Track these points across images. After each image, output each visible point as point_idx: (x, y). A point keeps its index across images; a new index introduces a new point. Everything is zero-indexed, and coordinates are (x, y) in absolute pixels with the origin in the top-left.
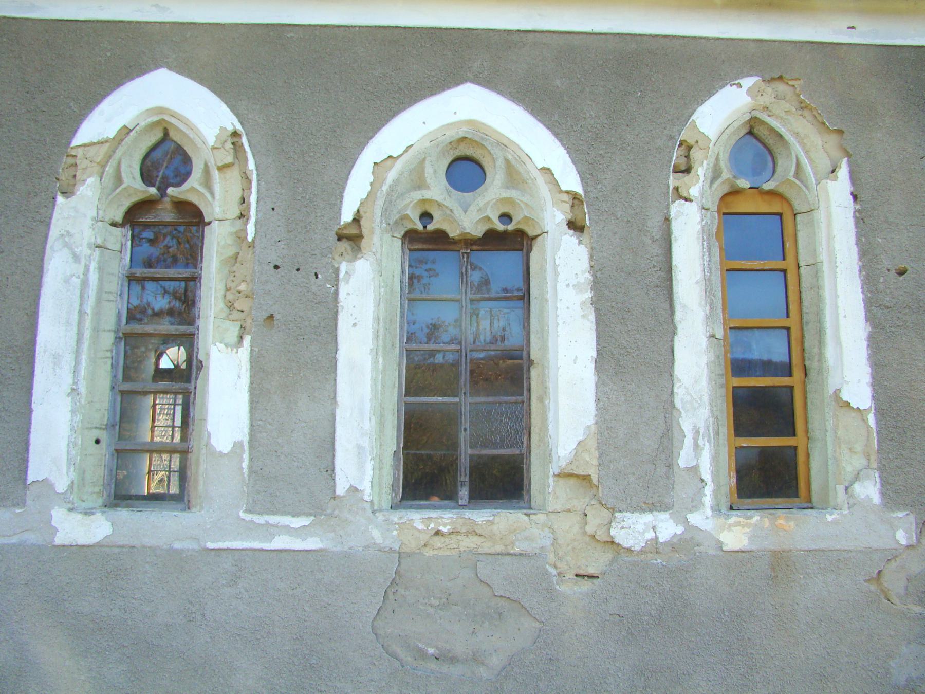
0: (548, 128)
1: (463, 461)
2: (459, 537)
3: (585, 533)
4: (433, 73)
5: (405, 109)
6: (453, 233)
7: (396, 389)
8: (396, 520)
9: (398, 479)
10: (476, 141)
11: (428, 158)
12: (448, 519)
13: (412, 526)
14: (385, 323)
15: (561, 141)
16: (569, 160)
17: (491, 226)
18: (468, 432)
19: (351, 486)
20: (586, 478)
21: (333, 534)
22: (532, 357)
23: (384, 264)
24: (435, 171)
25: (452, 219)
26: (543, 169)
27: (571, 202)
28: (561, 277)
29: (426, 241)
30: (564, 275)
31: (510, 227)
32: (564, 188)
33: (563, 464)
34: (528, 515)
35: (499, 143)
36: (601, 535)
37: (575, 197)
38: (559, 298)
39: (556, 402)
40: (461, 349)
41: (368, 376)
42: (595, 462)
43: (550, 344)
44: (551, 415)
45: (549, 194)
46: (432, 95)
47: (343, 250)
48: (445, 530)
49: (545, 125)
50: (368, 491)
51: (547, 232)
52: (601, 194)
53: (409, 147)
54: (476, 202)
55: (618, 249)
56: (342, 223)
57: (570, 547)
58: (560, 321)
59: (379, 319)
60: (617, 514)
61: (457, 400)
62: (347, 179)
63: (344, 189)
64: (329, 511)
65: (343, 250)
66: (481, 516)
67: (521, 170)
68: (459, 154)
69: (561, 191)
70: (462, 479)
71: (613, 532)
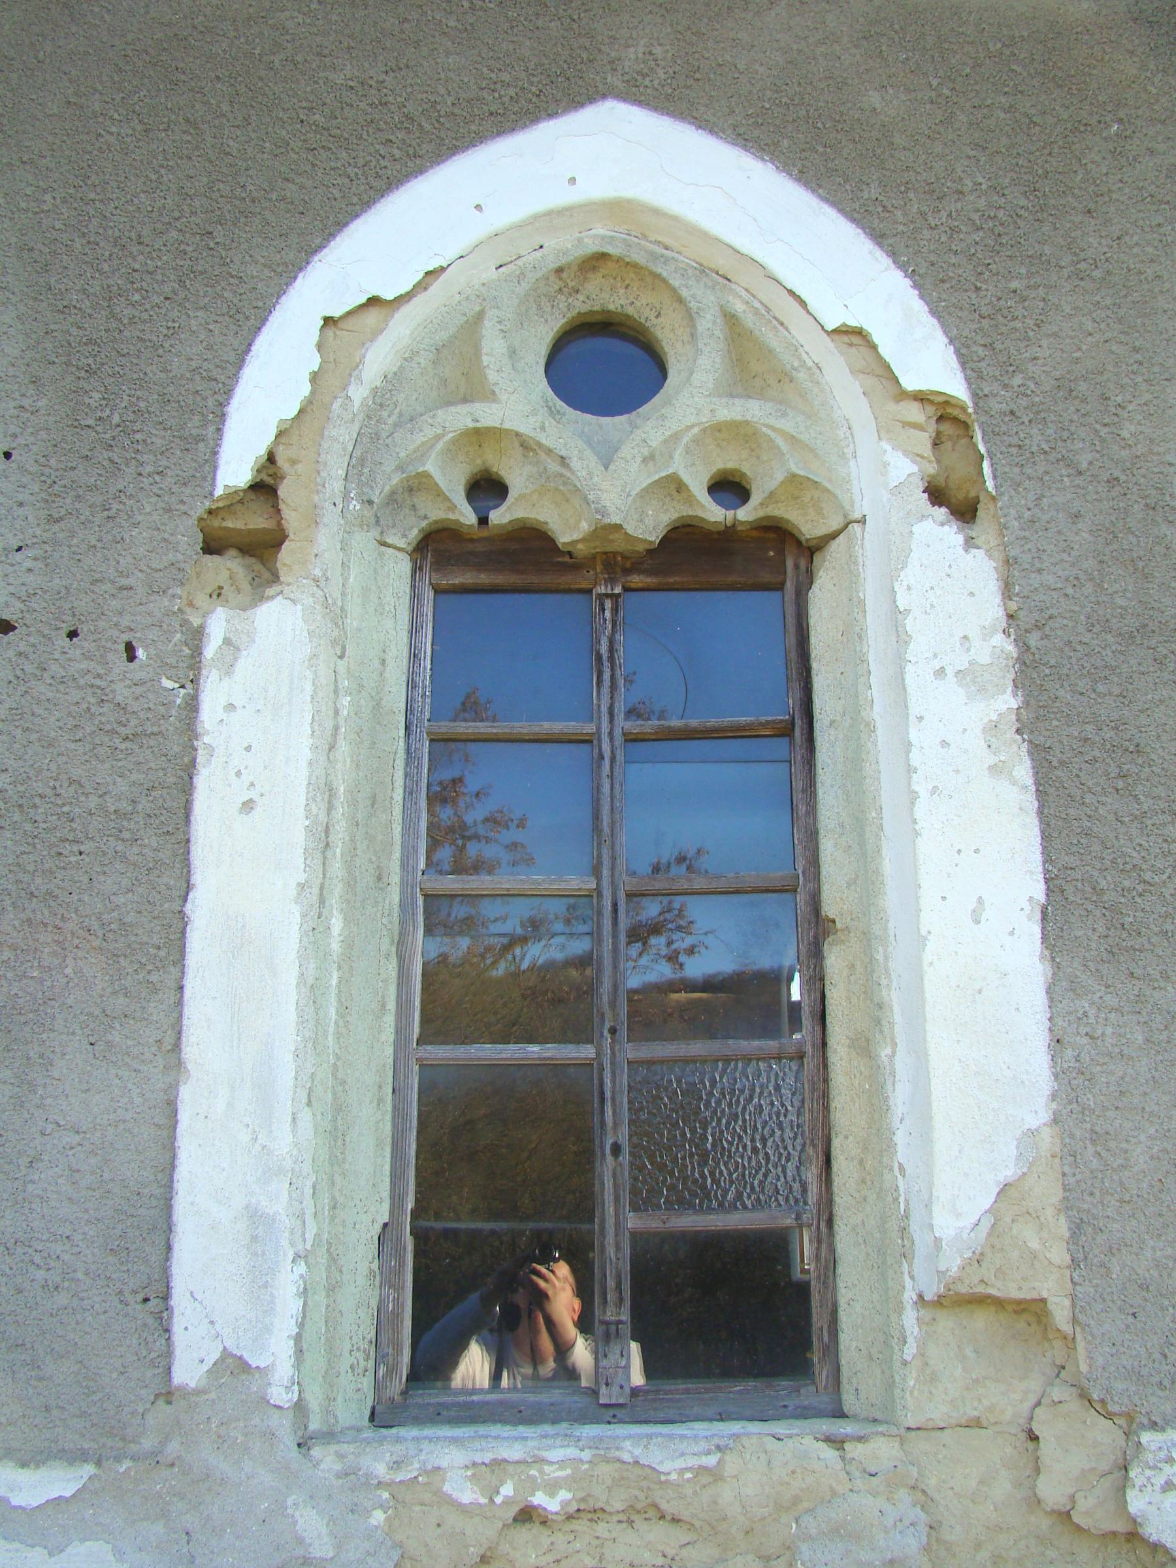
0: (853, 220)
1: (611, 1251)
2: (601, 1529)
3: (1035, 1501)
4: (506, 77)
5: (421, 171)
6: (569, 530)
7: (390, 1020)
8: (381, 1470)
9: (397, 1315)
10: (634, 266)
11: (491, 313)
12: (562, 1464)
13: (439, 1492)
14: (353, 803)
15: (893, 254)
16: (919, 307)
17: (687, 511)
18: (625, 1157)
19: (226, 1354)
20: (1033, 1311)
21: (159, 1528)
22: (829, 909)
23: (352, 623)
24: (512, 353)
27: (932, 427)
28: (918, 649)
29: (485, 562)
30: (926, 640)
31: (745, 514)
32: (910, 383)
33: (952, 1263)
34: (836, 1442)
35: (703, 270)
36: (1092, 1510)
37: (946, 416)
38: (914, 710)
39: (920, 1055)
40: (599, 890)
41: (289, 975)
42: (1059, 1254)
43: (888, 867)
44: (900, 1097)
45: (864, 403)
46: (500, 133)
47: (223, 578)
48: (550, 1503)
49: (841, 211)
50: (284, 1369)
51: (862, 521)
52: (1024, 402)
53: (432, 275)
54: (638, 435)
55: (1090, 564)
56: (219, 492)
57: (984, 1555)
58: (921, 786)
59: (331, 791)
60: (1146, 1437)
61: (587, 1052)
62: (240, 364)
63: (229, 393)
64: (148, 1443)
65: (223, 578)
66: (674, 1452)
67: (774, 343)
68: (585, 308)
69: (903, 395)
70: (610, 1315)
71: (1136, 1503)
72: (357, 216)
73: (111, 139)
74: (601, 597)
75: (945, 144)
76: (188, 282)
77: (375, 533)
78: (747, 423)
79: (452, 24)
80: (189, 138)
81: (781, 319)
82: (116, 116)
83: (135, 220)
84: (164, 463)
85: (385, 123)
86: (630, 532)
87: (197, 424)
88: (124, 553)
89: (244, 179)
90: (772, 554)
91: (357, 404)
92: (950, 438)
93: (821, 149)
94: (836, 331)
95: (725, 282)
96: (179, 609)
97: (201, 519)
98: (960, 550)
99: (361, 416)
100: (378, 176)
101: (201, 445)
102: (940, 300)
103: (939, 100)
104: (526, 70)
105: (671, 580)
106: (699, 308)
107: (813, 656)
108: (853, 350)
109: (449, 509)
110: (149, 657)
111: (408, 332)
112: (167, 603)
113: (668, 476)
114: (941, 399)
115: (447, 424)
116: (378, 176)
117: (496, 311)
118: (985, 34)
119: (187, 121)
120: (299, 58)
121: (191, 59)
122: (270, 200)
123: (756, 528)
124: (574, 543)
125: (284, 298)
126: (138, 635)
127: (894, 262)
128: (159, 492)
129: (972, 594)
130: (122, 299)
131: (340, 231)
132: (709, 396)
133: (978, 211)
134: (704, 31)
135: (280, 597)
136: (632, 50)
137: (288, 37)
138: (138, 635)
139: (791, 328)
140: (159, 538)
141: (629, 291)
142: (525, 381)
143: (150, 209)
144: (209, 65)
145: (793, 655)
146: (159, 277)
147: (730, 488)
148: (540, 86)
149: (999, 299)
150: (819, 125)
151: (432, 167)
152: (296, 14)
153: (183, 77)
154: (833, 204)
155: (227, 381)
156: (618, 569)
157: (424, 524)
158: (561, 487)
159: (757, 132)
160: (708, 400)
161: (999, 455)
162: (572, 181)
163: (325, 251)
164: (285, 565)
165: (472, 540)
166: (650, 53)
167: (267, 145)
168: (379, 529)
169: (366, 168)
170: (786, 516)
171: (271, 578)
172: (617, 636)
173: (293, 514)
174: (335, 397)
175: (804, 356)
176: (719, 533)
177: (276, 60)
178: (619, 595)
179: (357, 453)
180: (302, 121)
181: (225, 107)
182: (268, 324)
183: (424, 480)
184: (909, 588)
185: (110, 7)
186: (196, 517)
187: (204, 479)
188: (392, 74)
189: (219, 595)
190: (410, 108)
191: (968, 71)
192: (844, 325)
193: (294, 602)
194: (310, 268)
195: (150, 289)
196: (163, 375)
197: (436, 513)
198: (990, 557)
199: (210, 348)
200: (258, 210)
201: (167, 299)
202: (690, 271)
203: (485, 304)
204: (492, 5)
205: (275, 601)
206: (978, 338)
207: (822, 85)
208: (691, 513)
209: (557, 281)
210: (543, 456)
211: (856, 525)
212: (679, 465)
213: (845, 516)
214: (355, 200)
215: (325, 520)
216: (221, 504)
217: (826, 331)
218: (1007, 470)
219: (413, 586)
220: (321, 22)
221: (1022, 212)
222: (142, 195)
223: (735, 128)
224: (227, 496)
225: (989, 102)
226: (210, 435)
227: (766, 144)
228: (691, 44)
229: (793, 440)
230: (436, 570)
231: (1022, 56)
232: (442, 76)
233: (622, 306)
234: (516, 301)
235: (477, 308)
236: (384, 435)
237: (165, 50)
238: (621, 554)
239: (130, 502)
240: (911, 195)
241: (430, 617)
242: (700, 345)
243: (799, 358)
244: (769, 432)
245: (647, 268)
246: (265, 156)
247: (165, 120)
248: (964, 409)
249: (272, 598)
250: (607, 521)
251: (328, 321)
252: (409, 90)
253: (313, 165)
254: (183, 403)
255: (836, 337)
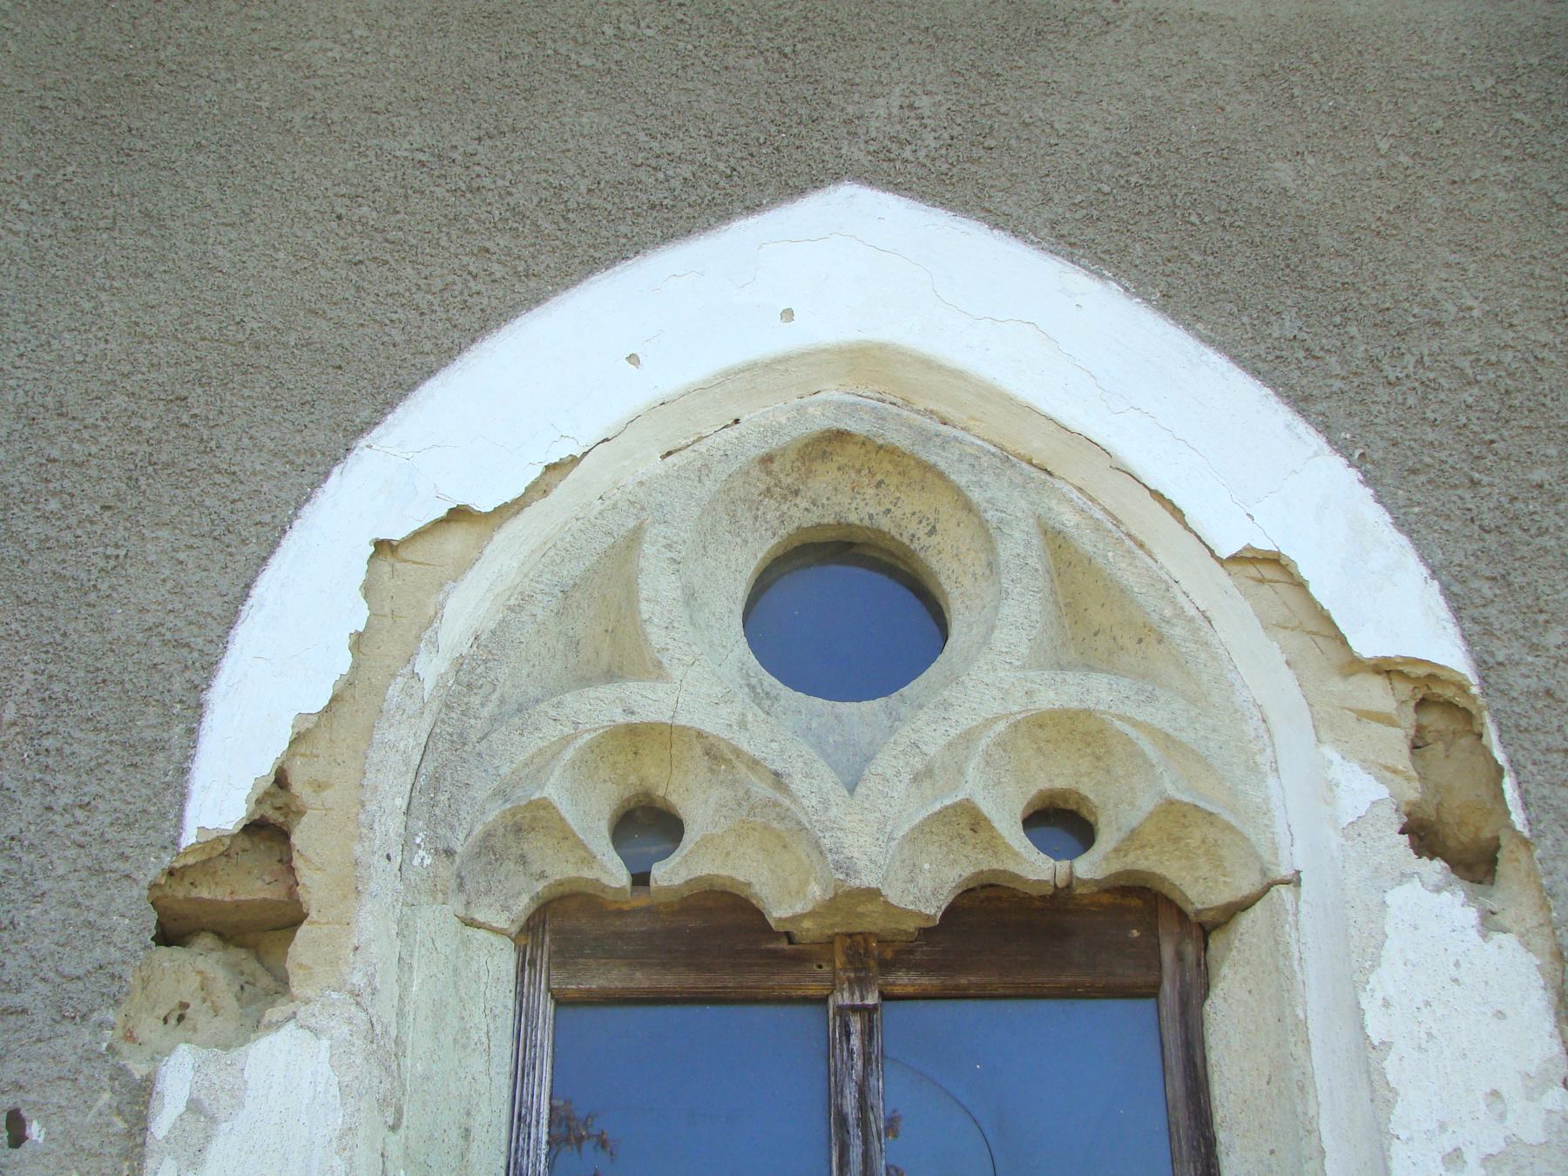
0: (1256, 373)
4: (675, 146)
5: (538, 299)
6: (789, 897)
10: (891, 452)
11: (654, 532)
15: (1325, 428)
16: (1376, 517)
17: (988, 863)
23: (414, 1065)
24: (690, 597)
25: (781, 826)
26: (1247, 559)
27: (1409, 718)
31: (1089, 867)
32: (1367, 645)
35: (1006, 458)
37: (1430, 698)
45: (1287, 677)
46: (668, 237)
49: (1235, 359)
51: (1295, 881)
54: (905, 734)
56: (189, 838)
62: (230, 619)
63: (210, 667)
67: (1129, 575)
68: (810, 520)
69: (1354, 665)
72: (431, 373)
73: (16, 243)
74: (842, 1010)
75: (1407, 245)
76: (143, 481)
77: (456, 905)
78: (1089, 713)
79: (586, 61)
80: (149, 242)
81: (1141, 537)
82: (24, 205)
83: (54, 376)
84: (93, 788)
85: (478, 221)
86: (894, 900)
87: (153, 721)
88: (13, 948)
89: (241, 310)
90: (1135, 933)
91: (429, 684)
92: (1440, 735)
93: (1198, 259)
94: (1234, 559)
95: (1044, 476)
96: (109, 1047)
97: (154, 886)
98: (1473, 935)
99: (435, 706)
100: (466, 306)
101: (160, 756)
102: (1411, 503)
103: (1393, 174)
104: (709, 135)
105: (964, 981)
106: (1001, 521)
107: (1217, 1119)
108: (1265, 589)
109: (583, 860)
110: (50, 1137)
111: (515, 564)
112: (88, 1038)
113: (954, 806)
114: (1421, 671)
115: (582, 719)
116: (466, 306)
117: (662, 527)
118: (1467, 63)
119: (147, 215)
120: (335, 115)
121: (153, 115)
122: (285, 345)
123: (1107, 891)
124: (796, 919)
125: (307, 508)
126: (33, 1097)
127: (1329, 441)
128: (82, 840)
129: (1500, 1015)
130: (29, 508)
131: (402, 397)
132: (1023, 667)
133: (1470, 353)
134: (999, 70)
135: (291, 1025)
136: (881, 101)
137: (317, 82)
138: (33, 1097)
139: (1157, 551)
140: (79, 921)
141: (882, 491)
142: (711, 644)
143: (79, 358)
144: (184, 125)
145: (1181, 1114)
146: (94, 473)
147: (1060, 821)
148: (733, 162)
149: (1514, 499)
150: (1194, 218)
151: (555, 293)
152: (330, 45)
153: (140, 145)
154: (1222, 347)
155: (209, 648)
156: (872, 963)
157: (540, 887)
158: (775, 824)
159: (1090, 233)
160: (1020, 674)
161: (1530, 767)
162: (788, 315)
163: (378, 431)
164: (301, 966)
165: (620, 913)
166: (912, 107)
167: (281, 255)
168: (463, 898)
169: (446, 294)
170: (1160, 870)
171: (273, 985)
172: (873, 1081)
173: (318, 876)
174: (393, 676)
175: (1181, 599)
176: (1043, 898)
177: (297, 118)
178: (874, 1008)
179: (429, 767)
180: (339, 217)
181: (211, 194)
182: (280, 552)
183: (542, 813)
184: (1386, 1004)
185: (18, 30)
186: (146, 884)
187: (163, 816)
188: (489, 142)
189: (181, 1018)
190: (519, 195)
191: (1439, 124)
192: (1249, 548)
193: (316, 1032)
194: (351, 458)
195: (77, 492)
196: (96, 638)
197: (561, 869)
198: (1527, 946)
199: (178, 590)
200: (264, 362)
201: (106, 508)
202: (985, 461)
203: (644, 515)
204: (650, 32)
205: (283, 1031)
206: (1481, 566)
207: (1197, 153)
208: (995, 867)
209: (763, 476)
210: (743, 770)
211: (1283, 888)
212: (973, 786)
213: (1264, 872)
214: (428, 346)
215: (373, 886)
216: (191, 860)
217: (1218, 559)
218: (1546, 791)
219: (519, 995)
220: (371, 58)
221: (1545, 353)
222: (66, 335)
223: (1053, 224)
224: (202, 846)
225: (1478, 173)
226: (175, 740)
227: (1107, 252)
228: (978, 91)
229: (1168, 741)
230: (560, 966)
231: (1532, 96)
232: (571, 145)
233: (871, 517)
234: (696, 512)
235: (631, 524)
236: (473, 737)
237: (109, 98)
238: (876, 935)
239: (29, 858)
240: (1353, 330)
241: (548, 1049)
242: (1005, 583)
243: (1173, 602)
244: (1127, 728)
245: (912, 456)
246: (278, 273)
247: (110, 213)
248: (1463, 688)
249: (276, 1026)
250: (855, 883)
251: (382, 547)
252: (517, 168)
253: (358, 289)
254: (128, 686)
255: (1235, 568)
